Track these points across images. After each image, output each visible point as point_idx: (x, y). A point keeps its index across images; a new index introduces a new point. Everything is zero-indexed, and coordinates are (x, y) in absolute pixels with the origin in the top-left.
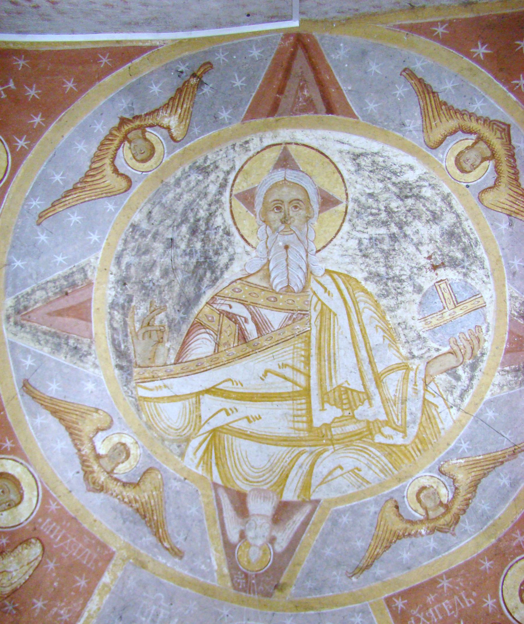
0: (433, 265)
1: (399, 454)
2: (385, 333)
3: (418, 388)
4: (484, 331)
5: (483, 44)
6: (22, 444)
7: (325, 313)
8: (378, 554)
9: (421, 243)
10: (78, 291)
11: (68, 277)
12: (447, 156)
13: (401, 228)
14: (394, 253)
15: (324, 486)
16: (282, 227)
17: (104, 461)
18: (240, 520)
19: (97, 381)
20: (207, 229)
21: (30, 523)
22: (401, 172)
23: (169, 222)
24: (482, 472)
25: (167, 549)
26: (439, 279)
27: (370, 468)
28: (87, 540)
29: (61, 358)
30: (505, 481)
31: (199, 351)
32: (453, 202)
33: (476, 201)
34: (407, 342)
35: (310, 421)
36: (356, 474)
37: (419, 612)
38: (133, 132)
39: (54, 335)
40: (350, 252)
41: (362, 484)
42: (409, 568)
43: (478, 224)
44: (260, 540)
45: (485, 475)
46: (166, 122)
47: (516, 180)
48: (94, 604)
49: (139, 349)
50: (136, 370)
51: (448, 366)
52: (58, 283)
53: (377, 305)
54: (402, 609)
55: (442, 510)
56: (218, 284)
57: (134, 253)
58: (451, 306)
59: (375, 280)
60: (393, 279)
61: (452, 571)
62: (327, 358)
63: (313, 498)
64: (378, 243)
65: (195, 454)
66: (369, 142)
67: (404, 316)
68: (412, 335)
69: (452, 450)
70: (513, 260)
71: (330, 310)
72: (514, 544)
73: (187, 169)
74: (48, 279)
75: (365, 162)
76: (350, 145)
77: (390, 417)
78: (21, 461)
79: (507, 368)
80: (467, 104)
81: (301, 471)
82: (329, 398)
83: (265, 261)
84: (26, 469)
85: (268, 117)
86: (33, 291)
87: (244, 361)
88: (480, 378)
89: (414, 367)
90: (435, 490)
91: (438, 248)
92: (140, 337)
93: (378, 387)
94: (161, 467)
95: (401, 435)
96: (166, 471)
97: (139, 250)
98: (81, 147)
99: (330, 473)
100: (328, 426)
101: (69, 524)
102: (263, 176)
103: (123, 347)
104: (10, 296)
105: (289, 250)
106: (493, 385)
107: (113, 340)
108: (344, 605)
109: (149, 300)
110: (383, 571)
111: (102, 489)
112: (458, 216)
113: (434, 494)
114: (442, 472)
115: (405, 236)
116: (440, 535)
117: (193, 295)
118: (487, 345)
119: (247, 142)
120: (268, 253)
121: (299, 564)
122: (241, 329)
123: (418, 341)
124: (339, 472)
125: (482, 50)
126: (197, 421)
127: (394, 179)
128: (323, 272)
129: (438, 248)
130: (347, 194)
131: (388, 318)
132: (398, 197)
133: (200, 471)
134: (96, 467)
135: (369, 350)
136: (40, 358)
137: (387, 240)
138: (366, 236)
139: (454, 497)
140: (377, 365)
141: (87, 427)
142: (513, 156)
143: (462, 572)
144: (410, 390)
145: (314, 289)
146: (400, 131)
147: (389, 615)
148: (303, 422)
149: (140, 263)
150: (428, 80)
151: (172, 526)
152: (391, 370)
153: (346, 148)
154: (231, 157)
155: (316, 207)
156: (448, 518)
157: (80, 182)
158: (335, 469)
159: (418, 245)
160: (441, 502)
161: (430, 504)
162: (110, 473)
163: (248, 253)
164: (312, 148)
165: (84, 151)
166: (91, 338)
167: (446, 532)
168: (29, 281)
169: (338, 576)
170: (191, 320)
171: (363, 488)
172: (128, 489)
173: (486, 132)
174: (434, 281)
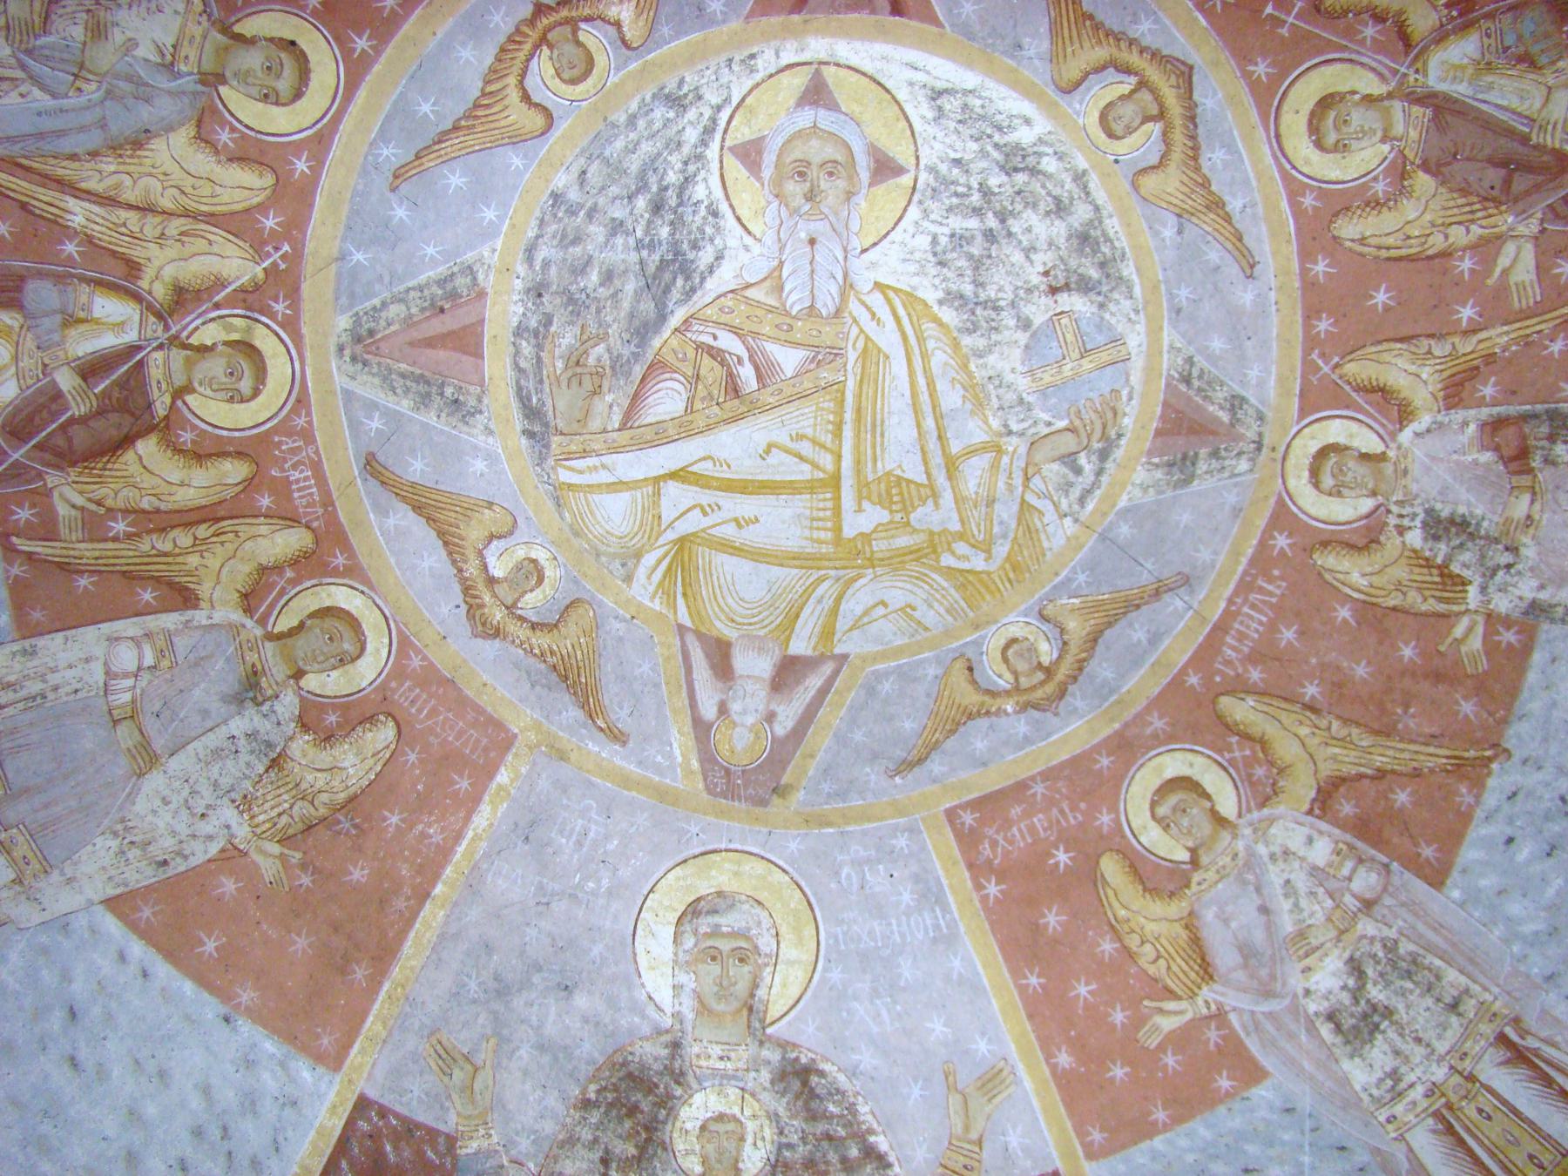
4: (1124, 398)
6: (364, 560)
7: (871, 354)
10: (461, 306)
11: (445, 280)
13: (1003, 221)
15: (855, 633)
16: (807, 207)
17: (501, 590)
18: (720, 685)
19: (491, 458)
20: (679, 205)
21: (377, 688)
23: (614, 190)
25: (601, 730)
28: (471, 715)
29: (430, 418)
30: (1139, 635)
31: (660, 409)
32: (1091, 185)
33: (1127, 186)
34: (1001, 408)
35: (838, 529)
36: (909, 616)
37: (997, 832)
38: (558, 29)
39: (420, 379)
40: (917, 256)
42: (984, 764)
43: (1129, 225)
44: (750, 714)
45: (1110, 625)
46: (613, 12)
47: (1195, 158)
48: (483, 818)
49: (561, 405)
50: (556, 440)
51: (1064, 450)
52: (426, 292)
53: (956, 345)
54: (971, 828)
55: (1040, 676)
56: (695, 298)
57: (555, 242)
58: (1076, 355)
60: (984, 304)
62: (870, 425)
63: (837, 651)
65: (649, 578)
66: (961, 70)
67: (1000, 365)
68: (1010, 397)
69: (1062, 583)
71: (879, 350)
72: (1148, 731)
73: (648, 99)
74: (410, 284)
75: (951, 104)
76: (928, 73)
78: (361, 587)
79: (1156, 460)
81: (819, 608)
82: (870, 493)
83: (776, 263)
84: (370, 602)
85: (791, 12)
86: (384, 304)
87: (734, 428)
89: (1011, 449)
91: (1062, 259)
92: (564, 384)
93: (950, 478)
94: (593, 597)
95: (983, 555)
96: (601, 604)
97: (564, 236)
98: (466, 54)
99: (866, 613)
100: (866, 537)
101: (441, 691)
102: (776, 116)
103: (534, 400)
104: (343, 312)
105: (816, 246)
107: (519, 389)
108: (882, 819)
109: (580, 322)
110: (945, 769)
111: (497, 633)
112: (1097, 209)
113: (1029, 650)
114: (1043, 617)
115: (1010, 234)
116: (1036, 714)
117: (652, 315)
119: (752, 56)
120: (781, 250)
121: (812, 756)
122: (730, 375)
124: (881, 611)
126: (653, 523)
127: (997, 138)
128: (871, 285)
129: (1062, 259)
130: (917, 158)
131: (972, 367)
132: (1002, 168)
133: (657, 605)
134: (487, 598)
135: (939, 417)
136: (393, 417)
137: (979, 238)
138: (946, 231)
139: (1060, 657)
141: (473, 534)
142: (1192, 119)
143: (1066, 773)
144: (1001, 484)
145: (855, 314)
146: (1013, 57)
147: (951, 835)
148: (825, 529)
149: (565, 260)
151: (611, 693)
152: (972, 451)
153: (920, 77)
154: (724, 80)
155: (865, 176)
156: (1050, 688)
157: (466, 117)
158: (875, 606)
159: (1029, 251)
161: (1022, 666)
162: (511, 608)
163: (747, 249)
164: (864, 74)
165: (473, 60)
166: (482, 386)
168: (377, 287)
169: (872, 775)
170: (650, 357)
172: (539, 633)
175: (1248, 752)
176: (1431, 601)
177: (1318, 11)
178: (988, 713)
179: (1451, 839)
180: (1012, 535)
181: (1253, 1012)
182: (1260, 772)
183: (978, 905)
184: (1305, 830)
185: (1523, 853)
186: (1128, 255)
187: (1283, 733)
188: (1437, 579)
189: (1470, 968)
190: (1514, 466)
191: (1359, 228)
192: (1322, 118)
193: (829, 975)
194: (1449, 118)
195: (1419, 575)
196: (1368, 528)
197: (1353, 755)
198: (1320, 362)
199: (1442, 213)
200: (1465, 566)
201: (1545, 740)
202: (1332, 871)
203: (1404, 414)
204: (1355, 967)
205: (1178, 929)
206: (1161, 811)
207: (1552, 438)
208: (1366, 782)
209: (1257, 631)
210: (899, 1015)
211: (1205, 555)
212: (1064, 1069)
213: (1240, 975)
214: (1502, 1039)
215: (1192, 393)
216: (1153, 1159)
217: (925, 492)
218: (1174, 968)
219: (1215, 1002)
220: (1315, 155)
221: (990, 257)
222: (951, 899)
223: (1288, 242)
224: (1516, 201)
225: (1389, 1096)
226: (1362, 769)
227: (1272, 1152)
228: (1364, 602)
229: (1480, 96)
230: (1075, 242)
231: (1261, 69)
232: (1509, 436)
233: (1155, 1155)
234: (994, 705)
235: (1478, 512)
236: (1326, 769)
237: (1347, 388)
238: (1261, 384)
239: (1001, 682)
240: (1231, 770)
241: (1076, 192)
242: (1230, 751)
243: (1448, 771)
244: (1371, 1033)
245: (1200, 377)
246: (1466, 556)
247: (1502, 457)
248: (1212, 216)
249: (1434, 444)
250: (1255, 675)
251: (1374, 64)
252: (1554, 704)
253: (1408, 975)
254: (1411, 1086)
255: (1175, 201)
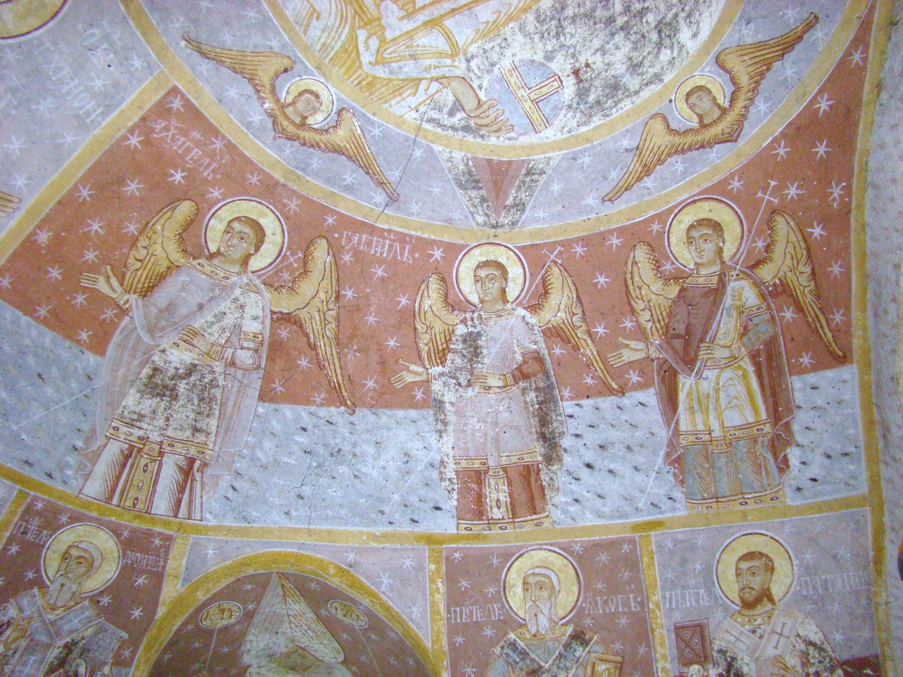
0: (579, 70)
1: (349, 61)
2: (493, 24)
3: (432, 71)
4: (509, 135)
5: (830, 107)
8: (222, 61)
9: (604, 54)
12: (708, 77)
13: (622, 28)
14: (592, 24)
22: (691, 23)
24: (352, 154)
26: (562, 78)
27: (323, 31)
30: (349, 179)
32: (653, 87)
33: (654, 111)
36: (311, 16)
41: (302, 25)
42: (220, 101)
43: (628, 116)
45: (350, 158)
51: (464, 101)
53: (525, 10)
55: (298, 121)
58: (533, 97)
59: (557, 5)
60: (560, 26)
61: (235, 146)
64: (603, 4)
68: (495, 57)
69: (369, 120)
70: (589, 156)
77: (391, 44)
79: (471, 164)
80: (765, 94)
88: (456, 137)
89: (456, 64)
90: (318, 109)
93: (425, 24)
95: (373, 60)
106: (451, 152)
112: (637, 93)
113: (314, 108)
114: (339, 113)
115: (613, 35)
116: (270, 125)
118: (493, 140)
123: (487, 64)
125: (823, 105)
127: (683, 15)
131: (511, 25)
132: (660, 22)
140: (453, 19)
142: (702, 147)
144: (428, 62)
146: (741, 18)
147: (159, 97)
150: (798, 48)
152: (448, 37)
156: (291, 129)
159: (602, 50)
160: (306, 118)
161: (300, 106)
167: (274, 130)
171: (297, 28)
173: (731, 117)
174: (560, 74)
175: (295, 265)
176: (427, 348)
177: (772, 213)
178: (258, 91)
179: (293, 399)
180: (393, 77)
181: (135, 328)
182: (286, 276)
183: (118, 136)
184: (261, 314)
185: (301, 439)
186: (608, 119)
187: (316, 283)
188: (440, 348)
189: (222, 431)
190: (517, 373)
191: (642, 259)
192: (707, 226)
193: (8, 50)
194: (711, 298)
195: (440, 339)
196: (461, 302)
197: (317, 326)
198: (556, 252)
199: (656, 304)
200: (453, 361)
201: (368, 431)
202: (242, 336)
203: (534, 308)
204: (191, 369)
205: (166, 263)
206: (236, 225)
207: (537, 389)
208: (305, 340)
209: (376, 252)
210: (9, 115)
211: (415, 208)
212: (36, 241)
213: (154, 311)
214: (192, 461)
215: (521, 177)
216: (13, 322)
217: (410, 7)
218: (139, 273)
219: (131, 305)
220: (684, 226)
221: (595, 24)
222: (114, 115)
223: (629, 219)
224: (668, 343)
225: (128, 421)
226: (312, 336)
227: (60, 383)
228: (414, 311)
229: (725, 312)
230: (612, 81)
231: (736, 184)
232: (535, 367)
233: (16, 322)
234: (265, 94)
235: (486, 360)
236: (303, 315)
237: (543, 272)
238: (536, 220)
239: (284, 94)
240: (280, 258)
241: (647, 77)
242: (292, 254)
243: (330, 384)
244: (158, 394)
245: (532, 181)
246: (459, 361)
247: (520, 366)
248: (640, 169)
249: (520, 328)
250: (347, 258)
251: (741, 250)
252: (389, 429)
253: (202, 400)
254: (140, 428)
255: (647, 144)
